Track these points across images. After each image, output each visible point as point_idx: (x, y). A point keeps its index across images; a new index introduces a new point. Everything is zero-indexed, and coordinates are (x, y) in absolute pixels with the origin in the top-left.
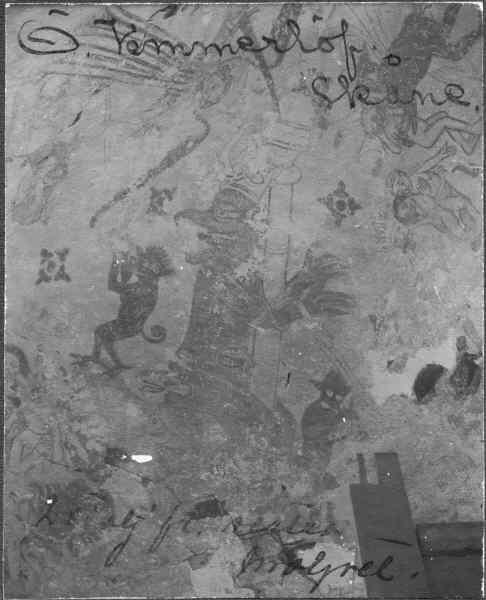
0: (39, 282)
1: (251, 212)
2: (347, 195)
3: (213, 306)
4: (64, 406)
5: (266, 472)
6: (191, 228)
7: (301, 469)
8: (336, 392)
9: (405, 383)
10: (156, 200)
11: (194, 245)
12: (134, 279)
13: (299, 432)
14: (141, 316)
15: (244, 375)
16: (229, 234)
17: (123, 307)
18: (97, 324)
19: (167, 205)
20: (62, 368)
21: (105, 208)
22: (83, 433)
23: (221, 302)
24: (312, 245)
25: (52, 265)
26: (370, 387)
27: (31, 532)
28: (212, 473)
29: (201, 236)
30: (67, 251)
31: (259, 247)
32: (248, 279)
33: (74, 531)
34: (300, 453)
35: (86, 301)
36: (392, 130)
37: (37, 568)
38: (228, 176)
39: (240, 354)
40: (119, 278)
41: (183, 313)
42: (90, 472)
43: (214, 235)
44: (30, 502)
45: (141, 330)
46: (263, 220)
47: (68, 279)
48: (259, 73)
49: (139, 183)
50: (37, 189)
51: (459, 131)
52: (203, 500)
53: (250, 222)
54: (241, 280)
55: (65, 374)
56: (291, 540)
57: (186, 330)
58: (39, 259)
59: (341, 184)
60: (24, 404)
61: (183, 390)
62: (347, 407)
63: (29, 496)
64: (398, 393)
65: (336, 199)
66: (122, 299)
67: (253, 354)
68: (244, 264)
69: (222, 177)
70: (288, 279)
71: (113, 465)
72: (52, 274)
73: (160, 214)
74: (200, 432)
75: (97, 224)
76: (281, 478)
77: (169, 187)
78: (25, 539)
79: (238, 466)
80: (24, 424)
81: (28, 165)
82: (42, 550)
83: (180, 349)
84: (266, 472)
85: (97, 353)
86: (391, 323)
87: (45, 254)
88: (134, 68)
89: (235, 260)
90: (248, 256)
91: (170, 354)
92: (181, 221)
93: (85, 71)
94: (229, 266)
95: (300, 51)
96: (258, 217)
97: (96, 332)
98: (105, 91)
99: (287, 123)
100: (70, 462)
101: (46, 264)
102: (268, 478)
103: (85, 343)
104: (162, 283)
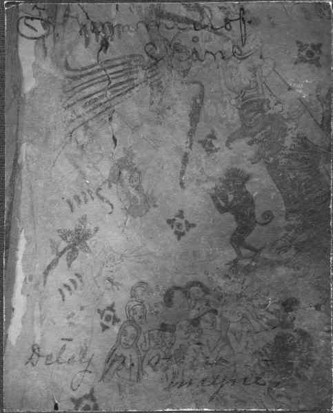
1: (265, 107)
3: (289, 176)
4: (241, 296)
6: (241, 144)
10: (207, 146)
11: (250, 152)
12: (231, 198)
14: (250, 214)
16: (263, 129)
21: (182, 173)
24: (317, 92)
25: (179, 225)
29: (250, 143)
30: (181, 212)
33: (295, 366)
38: (236, 98)
40: (223, 204)
41: (274, 194)
43: (257, 137)
45: (256, 222)
47: (194, 225)
49: (188, 145)
50: (131, 192)
53: (269, 112)
54: (293, 147)
55: (230, 278)
57: (283, 202)
58: (169, 226)
59: (298, 42)
60: (219, 309)
65: (304, 54)
69: (234, 102)
71: (292, 311)
77: (209, 132)
78: (268, 388)
80: (226, 321)
81: (113, 184)
82: (283, 389)
85: (239, 254)
87: (170, 222)
88: (118, 91)
90: (285, 130)
92: (232, 145)
93: (91, 115)
96: (272, 105)
98: (115, 115)
100: (266, 326)
101: (175, 227)
104: (248, 187)
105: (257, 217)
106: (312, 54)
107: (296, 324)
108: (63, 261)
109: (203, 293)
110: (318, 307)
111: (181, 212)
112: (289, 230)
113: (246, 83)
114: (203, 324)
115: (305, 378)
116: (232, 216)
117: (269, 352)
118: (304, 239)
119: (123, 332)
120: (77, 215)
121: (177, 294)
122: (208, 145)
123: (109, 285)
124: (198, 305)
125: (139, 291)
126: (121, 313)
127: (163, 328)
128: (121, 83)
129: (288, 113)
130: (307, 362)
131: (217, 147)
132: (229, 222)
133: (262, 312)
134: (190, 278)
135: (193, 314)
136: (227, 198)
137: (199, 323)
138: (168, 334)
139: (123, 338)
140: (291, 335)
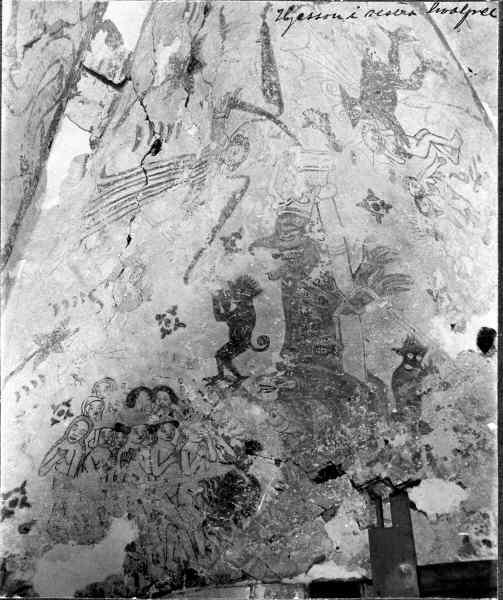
0: (163, 337)
2: (378, 199)
5: (370, 433)
7: (398, 423)
8: (415, 354)
9: (470, 341)
11: (273, 266)
12: (233, 307)
13: (390, 394)
15: (337, 358)
17: (231, 331)
18: (217, 349)
19: (239, 244)
20: (200, 392)
22: (226, 434)
23: (306, 303)
26: (443, 345)
27: (208, 516)
28: (326, 445)
29: (276, 256)
30: (175, 308)
31: (324, 252)
32: (321, 279)
33: (236, 510)
34: (395, 411)
35: (202, 336)
36: (391, 147)
37: (215, 541)
39: (332, 341)
40: (222, 311)
42: (237, 464)
43: (285, 253)
44: (202, 494)
45: (250, 344)
46: (319, 231)
47: (184, 326)
48: (269, 123)
51: (442, 145)
52: (324, 467)
53: (309, 234)
55: (203, 395)
56: (400, 482)
60: (181, 424)
61: (291, 384)
62: (427, 364)
63: (200, 490)
64: (466, 349)
65: (370, 203)
66: (229, 325)
67: (341, 339)
68: (315, 269)
69: (276, 206)
70: (354, 272)
71: (252, 454)
72: (172, 327)
73: (236, 251)
74: (310, 415)
75: (189, 280)
76: (383, 435)
79: (345, 435)
80: (185, 437)
82: (217, 528)
83: (283, 350)
84: (370, 433)
86: (444, 295)
89: (307, 267)
90: (317, 261)
91: (276, 357)
92: (255, 250)
94: (304, 275)
95: (251, 183)
97: (216, 357)
99: (309, 152)
102: (372, 437)
103: (210, 367)
104: (256, 302)
105: (252, 339)
106: (378, 209)
107: (251, 470)
108: (30, 364)
109: (169, 401)
110: (278, 462)
111: (175, 308)
112: (279, 369)
113: (298, 194)
114: (159, 433)
115: (241, 527)
116: (228, 328)
117: (216, 486)
118: (291, 387)
119: (74, 425)
120: (60, 318)
121: (143, 396)
122: (229, 245)
123: (72, 381)
124: (161, 412)
125: (103, 387)
126: (76, 410)
127: (118, 427)
128: (161, 183)
129: (327, 246)
130: (248, 511)
131: (239, 247)
132: (221, 332)
133: (222, 442)
134: (161, 382)
135: (153, 419)
136: (229, 305)
137: (156, 430)
138: (120, 434)
139: (72, 432)
140: (241, 478)
